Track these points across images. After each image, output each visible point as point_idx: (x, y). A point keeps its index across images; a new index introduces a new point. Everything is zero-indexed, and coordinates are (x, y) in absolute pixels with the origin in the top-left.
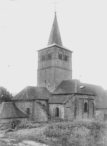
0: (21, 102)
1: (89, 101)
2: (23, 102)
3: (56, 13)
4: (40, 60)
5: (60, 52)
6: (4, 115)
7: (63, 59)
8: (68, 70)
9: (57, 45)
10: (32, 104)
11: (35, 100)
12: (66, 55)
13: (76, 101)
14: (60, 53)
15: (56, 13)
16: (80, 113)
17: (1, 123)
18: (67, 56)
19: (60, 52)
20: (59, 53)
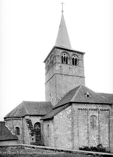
0: (17, 119)
1: (99, 113)
2: (20, 119)
3: (62, 11)
4: (46, 71)
5: (64, 54)
6: (4, 136)
7: (69, 63)
8: (84, 82)
9: (67, 51)
10: (21, 122)
11: (23, 117)
12: (73, 58)
13: (73, 113)
14: (65, 57)
15: (62, 11)
16: (83, 131)
17: (1, 147)
18: (76, 59)
19: (64, 54)
20: (62, 56)
